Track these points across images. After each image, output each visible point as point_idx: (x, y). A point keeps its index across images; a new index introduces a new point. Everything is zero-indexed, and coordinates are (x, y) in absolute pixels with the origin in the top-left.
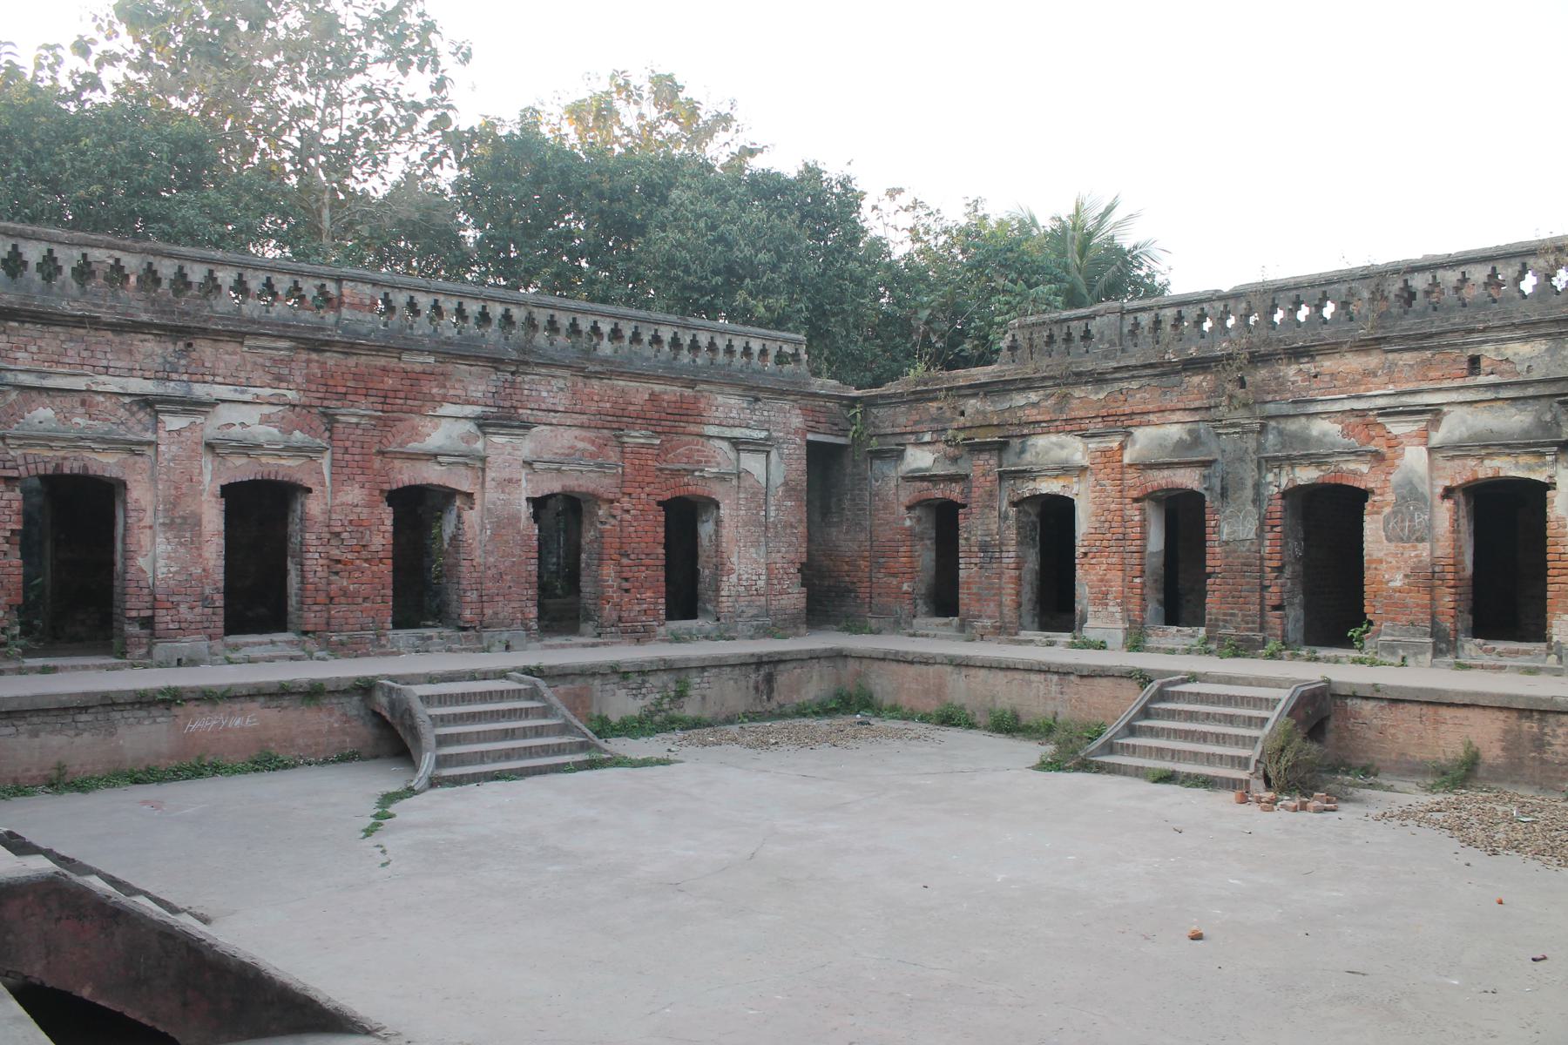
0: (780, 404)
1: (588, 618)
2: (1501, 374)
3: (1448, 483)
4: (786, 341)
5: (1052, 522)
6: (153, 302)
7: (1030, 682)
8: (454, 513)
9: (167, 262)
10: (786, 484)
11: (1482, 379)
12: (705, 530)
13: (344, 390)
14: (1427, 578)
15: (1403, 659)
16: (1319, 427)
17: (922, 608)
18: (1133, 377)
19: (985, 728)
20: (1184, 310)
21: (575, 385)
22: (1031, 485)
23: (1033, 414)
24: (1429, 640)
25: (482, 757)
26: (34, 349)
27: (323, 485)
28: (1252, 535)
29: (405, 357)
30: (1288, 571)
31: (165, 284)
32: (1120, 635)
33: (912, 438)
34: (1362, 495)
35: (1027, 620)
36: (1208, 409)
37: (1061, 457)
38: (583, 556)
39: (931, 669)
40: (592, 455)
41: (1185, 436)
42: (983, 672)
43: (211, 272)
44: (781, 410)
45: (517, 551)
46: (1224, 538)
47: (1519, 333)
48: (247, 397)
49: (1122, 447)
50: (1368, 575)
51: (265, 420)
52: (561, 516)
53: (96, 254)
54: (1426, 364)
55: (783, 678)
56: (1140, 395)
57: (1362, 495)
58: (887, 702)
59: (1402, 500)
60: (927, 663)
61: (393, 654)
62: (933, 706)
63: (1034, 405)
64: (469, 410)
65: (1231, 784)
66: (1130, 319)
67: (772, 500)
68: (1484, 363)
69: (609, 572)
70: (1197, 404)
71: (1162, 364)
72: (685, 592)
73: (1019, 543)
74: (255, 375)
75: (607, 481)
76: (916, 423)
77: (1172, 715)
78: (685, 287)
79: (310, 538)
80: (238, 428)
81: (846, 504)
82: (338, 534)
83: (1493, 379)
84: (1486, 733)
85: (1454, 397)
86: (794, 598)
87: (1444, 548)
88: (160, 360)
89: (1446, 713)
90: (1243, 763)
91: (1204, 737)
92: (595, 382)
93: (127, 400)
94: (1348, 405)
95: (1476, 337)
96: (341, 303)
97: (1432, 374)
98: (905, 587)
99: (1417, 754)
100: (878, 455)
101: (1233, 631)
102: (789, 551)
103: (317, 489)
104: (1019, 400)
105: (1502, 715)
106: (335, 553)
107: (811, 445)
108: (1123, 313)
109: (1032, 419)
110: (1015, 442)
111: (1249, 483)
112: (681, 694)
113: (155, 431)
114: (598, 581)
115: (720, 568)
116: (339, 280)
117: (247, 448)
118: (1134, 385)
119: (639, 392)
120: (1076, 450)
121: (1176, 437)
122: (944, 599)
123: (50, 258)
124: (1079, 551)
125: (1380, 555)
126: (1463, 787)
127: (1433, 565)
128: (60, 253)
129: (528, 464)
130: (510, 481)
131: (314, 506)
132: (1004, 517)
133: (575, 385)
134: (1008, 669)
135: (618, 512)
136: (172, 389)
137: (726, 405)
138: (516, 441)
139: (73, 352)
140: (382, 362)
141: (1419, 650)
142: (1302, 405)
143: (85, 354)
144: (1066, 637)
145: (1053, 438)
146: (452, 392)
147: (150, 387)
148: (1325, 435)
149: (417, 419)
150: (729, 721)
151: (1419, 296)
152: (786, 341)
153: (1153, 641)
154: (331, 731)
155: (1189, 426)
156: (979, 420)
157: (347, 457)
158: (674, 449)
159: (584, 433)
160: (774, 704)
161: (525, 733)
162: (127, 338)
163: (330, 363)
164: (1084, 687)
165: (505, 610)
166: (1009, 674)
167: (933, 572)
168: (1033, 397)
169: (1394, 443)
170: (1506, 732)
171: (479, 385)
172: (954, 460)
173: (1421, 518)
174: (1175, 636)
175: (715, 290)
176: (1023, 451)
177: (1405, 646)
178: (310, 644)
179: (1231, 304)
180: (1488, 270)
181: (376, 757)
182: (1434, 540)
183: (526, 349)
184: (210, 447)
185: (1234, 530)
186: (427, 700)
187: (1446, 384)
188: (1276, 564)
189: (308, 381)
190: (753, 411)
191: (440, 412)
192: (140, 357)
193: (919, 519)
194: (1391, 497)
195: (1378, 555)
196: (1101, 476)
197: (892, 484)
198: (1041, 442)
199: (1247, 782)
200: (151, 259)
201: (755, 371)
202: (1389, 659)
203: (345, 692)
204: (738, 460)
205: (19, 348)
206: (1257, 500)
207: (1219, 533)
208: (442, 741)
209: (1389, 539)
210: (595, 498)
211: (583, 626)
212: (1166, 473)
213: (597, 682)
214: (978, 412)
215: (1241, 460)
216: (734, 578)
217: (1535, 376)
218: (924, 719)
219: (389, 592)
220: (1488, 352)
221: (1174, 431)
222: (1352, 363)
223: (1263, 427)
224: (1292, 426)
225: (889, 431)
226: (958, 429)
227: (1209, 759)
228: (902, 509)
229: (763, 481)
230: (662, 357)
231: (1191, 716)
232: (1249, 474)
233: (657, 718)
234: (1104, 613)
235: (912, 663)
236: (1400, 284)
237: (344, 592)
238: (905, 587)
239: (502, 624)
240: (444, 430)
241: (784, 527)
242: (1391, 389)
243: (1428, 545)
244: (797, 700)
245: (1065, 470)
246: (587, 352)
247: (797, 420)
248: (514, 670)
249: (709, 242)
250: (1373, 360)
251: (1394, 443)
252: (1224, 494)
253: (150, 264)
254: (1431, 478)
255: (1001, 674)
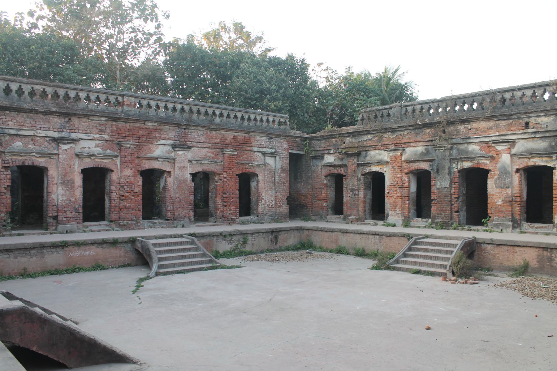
0: (280, 139)
1: (212, 216)
2: (537, 128)
3: (518, 167)
4: (282, 117)
5: (377, 181)
6: (57, 104)
7: (369, 238)
8: (164, 178)
9: (62, 90)
10: (282, 168)
11: (530, 130)
12: (253, 184)
13: (124, 135)
14: (510, 201)
15: (502, 230)
16: (472, 147)
17: (330, 212)
18: (405, 130)
19: (353, 255)
20: (423, 106)
21: (207, 133)
22: (369, 168)
23: (370, 143)
24: (511, 223)
25: (174, 265)
26: (15, 121)
27: (117, 169)
28: (448, 186)
29: (146, 123)
30: (461, 199)
31: (61, 98)
32: (401, 221)
33: (327, 152)
34: (487, 172)
35: (368, 216)
36: (432, 141)
37: (380, 158)
38: (210, 194)
39: (334, 234)
40: (213, 158)
41: (424, 151)
42: (352, 235)
43: (77, 93)
44: (280, 142)
45: (186, 192)
46: (438, 187)
47: (543, 114)
48: (90, 138)
49: (401, 155)
50: (489, 200)
51: (97, 146)
52: (202, 179)
53: (37, 87)
54: (510, 125)
55: (281, 237)
56: (408, 136)
57: (487, 172)
58: (318, 246)
59: (501, 174)
60: (332, 232)
61: (143, 229)
62: (334, 247)
63: (370, 140)
64: (169, 142)
65: (440, 274)
66: (404, 109)
67: (277, 174)
68: (530, 125)
69: (219, 200)
70: (428, 139)
71: (415, 125)
72: (246, 207)
73: (365, 189)
74: (93, 130)
75: (218, 167)
76: (328, 146)
77: (419, 250)
78: (246, 98)
79: (113, 188)
80: (87, 149)
81: (303, 175)
82: (123, 186)
83: (534, 130)
84: (531, 256)
85: (520, 136)
86: (285, 208)
87: (516, 190)
88: (59, 125)
89: (517, 249)
90: (444, 267)
91: (431, 258)
92: (214, 132)
93: (48, 139)
94: (482, 140)
95: (528, 115)
96: (124, 104)
97: (512, 128)
98: (324, 205)
99: (507, 264)
100: (314, 158)
101: (441, 220)
102: (283, 192)
103: (115, 170)
104: (365, 138)
105: (537, 250)
106: (122, 193)
107: (291, 154)
108: (402, 107)
109: (369, 145)
110: (363, 153)
111: (447, 167)
112: (245, 243)
113: (58, 150)
114: (215, 203)
115: (258, 198)
116: (123, 96)
117: (90, 156)
118: (406, 132)
119: (229, 136)
120: (385, 156)
121: (421, 151)
122: (338, 209)
123: (20, 89)
124: (386, 192)
125: (494, 193)
126: (523, 275)
127: (512, 196)
128: (24, 87)
129: (190, 161)
130: (184, 167)
131: (114, 176)
132: (359, 180)
133: (207, 133)
134: (361, 233)
135: (222, 178)
136: (64, 135)
137: (260, 140)
138: (186, 153)
139: (29, 122)
140: (138, 125)
141: (507, 227)
142: (466, 140)
143: (33, 123)
144: (381, 222)
145: (377, 152)
146: (163, 136)
147: (56, 134)
148: (474, 150)
149: (151, 145)
150: (262, 252)
151: (507, 100)
152: (282, 117)
153: (412, 224)
154: (121, 256)
155: (425, 147)
156: (351, 145)
157: (126, 159)
158: (242, 156)
159: (210, 150)
160: (278, 246)
161: (189, 257)
162: (48, 117)
163: (120, 125)
164: (388, 240)
165: (182, 213)
166: (361, 235)
167: (334, 199)
168: (370, 137)
169: (498, 153)
170: (538, 256)
171: (173, 133)
172: (342, 159)
173: (508, 180)
174: (420, 222)
175: (256, 99)
176: (366, 156)
177: (502, 225)
178: (113, 225)
179: (440, 104)
180: (532, 91)
181: (136, 265)
182: (513, 188)
183: (189, 120)
184: (77, 155)
185: (441, 184)
186: (155, 245)
187: (517, 132)
188: (456, 196)
189: (112, 132)
190: (270, 142)
191: (159, 143)
192: (52, 123)
193: (329, 181)
194: (497, 172)
195: (493, 193)
196: (394, 165)
197: (320, 168)
198: (373, 153)
199: (446, 274)
200: (56, 89)
201: (270, 128)
202: (496, 230)
203: (125, 242)
204: (265, 160)
205: (9, 121)
206: (449, 173)
207: (436, 185)
208: (160, 259)
209: (496, 187)
210: (214, 173)
211: (210, 219)
212: (417, 164)
213: (215, 239)
214: (350, 142)
215: (444, 159)
216: (263, 202)
217: (549, 129)
218: (331, 251)
219: (141, 207)
220: (532, 121)
221: (420, 149)
222: (484, 125)
223: (452, 147)
224: (462, 147)
225: (318, 149)
226: (343, 148)
227: (433, 265)
228: (323, 177)
229: (274, 167)
230: (238, 123)
231: (426, 250)
232: (447, 164)
233: (236, 251)
234: (395, 214)
235: (327, 231)
236: (501, 97)
237: (125, 207)
238: (324, 205)
239: (181, 218)
240: (160, 149)
241: (281, 183)
242: (497, 134)
243: (510, 189)
244: (286, 245)
245: (381, 163)
246: (211, 121)
247: (285, 145)
248: (185, 234)
249: (254, 82)
250: (491, 124)
251: (498, 153)
252: (438, 171)
253: (56, 91)
254: (512, 166)
255: (358, 235)
